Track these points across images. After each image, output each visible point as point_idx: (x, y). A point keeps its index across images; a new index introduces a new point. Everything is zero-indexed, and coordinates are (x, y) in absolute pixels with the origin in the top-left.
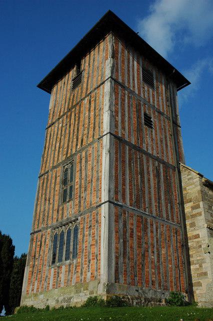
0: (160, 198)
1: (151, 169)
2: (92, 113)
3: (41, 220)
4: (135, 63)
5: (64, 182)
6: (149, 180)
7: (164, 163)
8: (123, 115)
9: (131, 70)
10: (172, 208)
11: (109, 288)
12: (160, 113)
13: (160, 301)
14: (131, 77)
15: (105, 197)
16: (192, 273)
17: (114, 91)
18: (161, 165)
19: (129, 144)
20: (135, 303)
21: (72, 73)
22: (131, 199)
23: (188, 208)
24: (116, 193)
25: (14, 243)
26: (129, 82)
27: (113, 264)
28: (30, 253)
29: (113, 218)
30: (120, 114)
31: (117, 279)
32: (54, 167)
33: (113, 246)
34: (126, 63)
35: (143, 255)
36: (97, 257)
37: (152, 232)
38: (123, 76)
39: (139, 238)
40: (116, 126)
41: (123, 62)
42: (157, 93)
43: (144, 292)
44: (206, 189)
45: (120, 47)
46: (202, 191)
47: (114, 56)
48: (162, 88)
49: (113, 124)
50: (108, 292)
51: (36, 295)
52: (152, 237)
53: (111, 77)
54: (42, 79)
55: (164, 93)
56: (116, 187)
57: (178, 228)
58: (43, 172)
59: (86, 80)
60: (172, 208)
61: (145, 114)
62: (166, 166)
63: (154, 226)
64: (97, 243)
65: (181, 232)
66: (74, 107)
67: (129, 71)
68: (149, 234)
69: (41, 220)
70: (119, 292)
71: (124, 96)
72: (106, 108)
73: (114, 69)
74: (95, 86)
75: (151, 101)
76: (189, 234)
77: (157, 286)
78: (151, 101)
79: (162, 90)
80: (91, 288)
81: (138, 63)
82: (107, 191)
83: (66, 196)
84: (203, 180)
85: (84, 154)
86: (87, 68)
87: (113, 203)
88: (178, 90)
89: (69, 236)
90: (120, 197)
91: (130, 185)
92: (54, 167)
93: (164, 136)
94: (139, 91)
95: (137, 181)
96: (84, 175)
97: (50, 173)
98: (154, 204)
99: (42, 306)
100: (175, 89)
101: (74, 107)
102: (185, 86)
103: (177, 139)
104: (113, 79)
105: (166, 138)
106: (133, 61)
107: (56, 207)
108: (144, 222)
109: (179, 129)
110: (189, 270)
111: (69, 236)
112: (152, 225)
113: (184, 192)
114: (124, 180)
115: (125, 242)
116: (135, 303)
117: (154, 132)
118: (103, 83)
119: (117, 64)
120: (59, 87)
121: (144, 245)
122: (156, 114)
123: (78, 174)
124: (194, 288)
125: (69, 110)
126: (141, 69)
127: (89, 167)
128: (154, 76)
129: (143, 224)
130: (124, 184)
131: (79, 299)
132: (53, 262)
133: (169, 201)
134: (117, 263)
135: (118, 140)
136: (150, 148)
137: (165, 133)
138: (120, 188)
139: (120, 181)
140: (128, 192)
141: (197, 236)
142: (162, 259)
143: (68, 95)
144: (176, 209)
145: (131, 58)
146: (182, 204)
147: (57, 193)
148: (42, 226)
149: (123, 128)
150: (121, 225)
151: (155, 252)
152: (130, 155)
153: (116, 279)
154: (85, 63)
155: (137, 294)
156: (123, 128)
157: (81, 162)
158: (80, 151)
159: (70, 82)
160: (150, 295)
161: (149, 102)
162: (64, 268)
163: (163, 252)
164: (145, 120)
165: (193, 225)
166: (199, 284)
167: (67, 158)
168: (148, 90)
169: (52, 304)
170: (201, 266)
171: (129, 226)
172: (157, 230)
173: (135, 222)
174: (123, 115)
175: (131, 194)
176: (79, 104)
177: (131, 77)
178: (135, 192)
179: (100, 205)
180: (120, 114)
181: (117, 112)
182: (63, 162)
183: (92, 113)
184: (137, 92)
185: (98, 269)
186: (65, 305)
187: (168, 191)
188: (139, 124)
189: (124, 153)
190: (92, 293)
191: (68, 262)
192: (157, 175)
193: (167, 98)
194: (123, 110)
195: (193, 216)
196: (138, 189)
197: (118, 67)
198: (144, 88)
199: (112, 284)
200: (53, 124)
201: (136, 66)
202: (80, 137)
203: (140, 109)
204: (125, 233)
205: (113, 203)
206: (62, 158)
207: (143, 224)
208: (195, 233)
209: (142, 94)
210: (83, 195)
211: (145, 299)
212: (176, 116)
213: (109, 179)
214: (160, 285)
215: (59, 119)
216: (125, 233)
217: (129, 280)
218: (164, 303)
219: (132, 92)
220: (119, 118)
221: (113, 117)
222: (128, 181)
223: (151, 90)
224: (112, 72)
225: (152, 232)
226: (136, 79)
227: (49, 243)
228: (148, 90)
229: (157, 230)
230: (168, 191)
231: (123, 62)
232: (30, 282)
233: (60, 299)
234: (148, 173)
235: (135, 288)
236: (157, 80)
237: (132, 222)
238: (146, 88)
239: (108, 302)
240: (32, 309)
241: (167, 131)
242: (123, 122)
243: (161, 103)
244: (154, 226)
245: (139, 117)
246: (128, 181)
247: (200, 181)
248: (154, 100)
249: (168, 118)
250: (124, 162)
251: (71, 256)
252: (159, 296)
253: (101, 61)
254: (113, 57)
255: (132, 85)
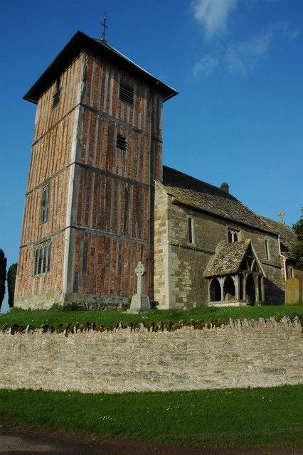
0: (126, 218)
1: (119, 191)
2: (65, 139)
3: (27, 236)
4: (112, 80)
5: (44, 203)
6: (116, 202)
7: (135, 183)
8: (92, 141)
9: (106, 90)
10: (140, 226)
11: (67, 297)
12: (137, 131)
13: (117, 305)
14: (105, 98)
15: (68, 224)
16: (155, 282)
17: (83, 118)
18: (132, 186)
19: (96, 170)
20: (91, 308)
21: (53, 88)
22: (94, 222)
23: (157, 223)
24: (79, 218)
25: (6, 256)
26: (102, 105)
27: (73, 277)
28: (20, 262)
29: (74, 241)
30: (88, 142)
31: (75, 289)
32: (37, 188)
33: (73, 264)
34: (100, 84)
35: (104, 270)
36: (61, 271)
37: (115, 249)
38: (95, 99)
39: (100, 256)
40: (83, 155)
41: (97, 83)
42: (136, 109)
43: (101, 299)
44: (175, 208)
45: (95, 65)
46: (169, 210)
47: (86, 78)
48: (143, 102)
49: (80, 153)
50: (66, 300)
51: (23, 299)
52: (115, 254)
53: (81, 104)
54: (69, 40)
55: (145, 107)
56: (79, 213)
57: (145, 244)
58: (29, 191)
59: (63, 100)
60: (140, 226)
61: (119, 136)
62: (138, 186)
63: (118, 244)
64: (61, 262)
65: (148, 247)
66: (53, 128)
67: (103, 91)
68: (112, 252)
69: (27, 236)
70: (76, 299)
71: (95, 121)
72: (74, 137)
73: (85, 93)
74: (68, 110)
75: (128, 119)
76: (156, 248)
77: (115, 293)
78: (128, 119)
79: (143, 105)
80: (55, 297)
81: (116, 79)
82: (70, 217)
83: (44, 217)
84: (173, 199)
85: (57, 178)
86: (64, 86)
87: (75, 228)
88: (164, 101)
89: (45, 250)
90: (82, 221)
91: (94, 210)
92: (37, 188)
93: (139, 157)
94: (114, 111)
95: (102, 205)
96: (56, 200)
97: (34, 193)
98: (120, 224)
99: (26, 308)
100: (161, 100)
101: (53, 128)
102: (173, 96)
103: (156, 155)
104: (83, 105)
105: (142, 156)
106: (110, 79)
107: (37, 226)
108: (106, 241)
109: (159, 144)
110: (153, 279)
111: (45, 250)
112: (115, 243)
113: (155, 210)
114: (88, 206)
115: (85, 261)
116: (91, 308)
117: (126, 155)
118: (74, 109)
119: (89, 87)
120: (76, 66)
121: (106, 261)
122: (133, 133)
123: (52, 199)
124: (155, 294)
125: (49, 130)
126: (119, 87)
127: (60, 193)
128: (135, 91)
129: (105, 243)
130: (88, 209)
131: (48, 305)
132: (35, 273)
133: (138, 219)
134: (76, 278)
135: (83, 168)
136: (120, 171)
137: (142, 152)
138: (83, 213)
139: (84, 207)
140: (92, 216)
141: (161, 251)
142: (124, 271)
143: (49, 114)
144: (145, 226)
145: (107, 76)
146: (152, 221)
147: (38, 213)
148: (27, 242)
149: (91, 155)
150: (82, 246)
151: (117, 267)
152: (96, 181)
153: (74, 290)
154: (64, 77)
155: (94, 301)
156: (91, 155)
157: (54, 187)
158: (54, 176)
159: (52, 99)
160: (107, 301)
161: (125, 121)
162: (41, 280)
163: (126, 265)
164: (117, 143)
165: (159, 240)
166: (158, 291)
167: (46, 181)
168: (125, 109)
169: (33, 307)
170: (161, 277)
171: (90, 246)
172: (120, 248)
173: (96, 242)
174: (92, 141)
175: (94, 218)
176: (56, 126)
177: (105, 98)
178: (99, 215)
179: (65, 229)
180: (88, 142)
181: (85, 140)
182: (43, 184)
183: (65, 139)
184: (111, 114)
185: (62, 282)
186: (40, 308)
187: (138, 210)
188: (110, 148)
189: (90, 180)
190: (56, 300)
191: (44, 274)
192: (127, 196)
193: (148, 112)
194: (92, 136)
195: (160, 233)
196: (102, 212)
197: (89, 90)
198: (120, 107)
199: (70, 294)
200: (37, 142)
201: (112, 84)
202: (55, 161)
203: (113, 132)
204: (85, 252)
205: (75, 228)
206: (42, 180)
207: (105, 243)
208: (160, 248)
209: (117, 115)
210: (55, 218)
211: (101, 305)
212: (159, 131)
213: (72, 207)
214: (119, 293)
215: (42, 138)
216: (85, 252)
217: (87, 290)
218: (120, 307)
219: (105, 115)
220: (87, 147)
221: (79, 145)
222: (92, 206)
223: (129, 108)
224: (82, 98)
225: (115, 249)
226: (111, 99)
227: (32, 257)
228: (125, 109)
229: (120, 248)
230: (138, 210)
231: (97, 83)
232: (19, 289)
233: (38, 303)
234: (116, 196)
235: (92, 296)
236: (138, 95)
237: (94, 243)
238: (123, 107)
239: (65, 307)
240: (21, 310)
241: (145, 149)
242: (91, 148)
243: (140, 121)
244: (118, 244)
245: (110, 141)
246: (92, 206)
247: (168, 200)
248: (131, 118)
249: (147, 135)
250: (89, 188)
251: (46, 270)
252: (116, 302)
253: (73, 80)
254: (84, 80)
255: (105, 107)
